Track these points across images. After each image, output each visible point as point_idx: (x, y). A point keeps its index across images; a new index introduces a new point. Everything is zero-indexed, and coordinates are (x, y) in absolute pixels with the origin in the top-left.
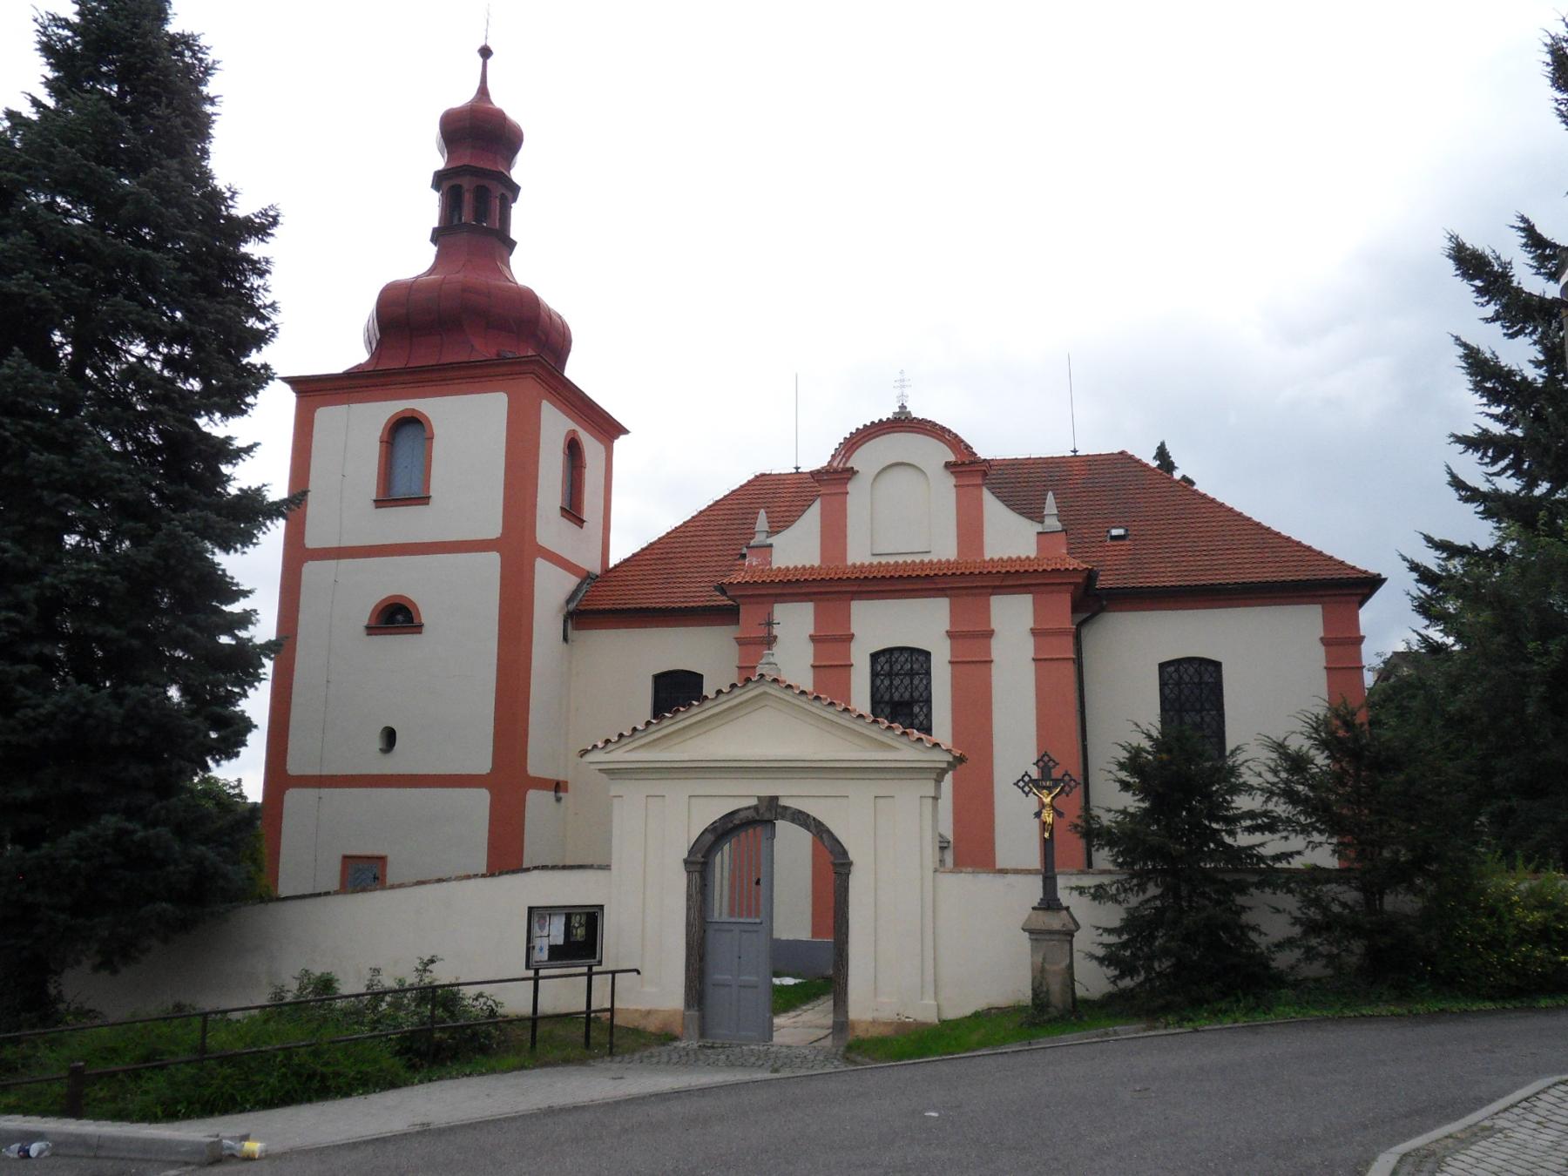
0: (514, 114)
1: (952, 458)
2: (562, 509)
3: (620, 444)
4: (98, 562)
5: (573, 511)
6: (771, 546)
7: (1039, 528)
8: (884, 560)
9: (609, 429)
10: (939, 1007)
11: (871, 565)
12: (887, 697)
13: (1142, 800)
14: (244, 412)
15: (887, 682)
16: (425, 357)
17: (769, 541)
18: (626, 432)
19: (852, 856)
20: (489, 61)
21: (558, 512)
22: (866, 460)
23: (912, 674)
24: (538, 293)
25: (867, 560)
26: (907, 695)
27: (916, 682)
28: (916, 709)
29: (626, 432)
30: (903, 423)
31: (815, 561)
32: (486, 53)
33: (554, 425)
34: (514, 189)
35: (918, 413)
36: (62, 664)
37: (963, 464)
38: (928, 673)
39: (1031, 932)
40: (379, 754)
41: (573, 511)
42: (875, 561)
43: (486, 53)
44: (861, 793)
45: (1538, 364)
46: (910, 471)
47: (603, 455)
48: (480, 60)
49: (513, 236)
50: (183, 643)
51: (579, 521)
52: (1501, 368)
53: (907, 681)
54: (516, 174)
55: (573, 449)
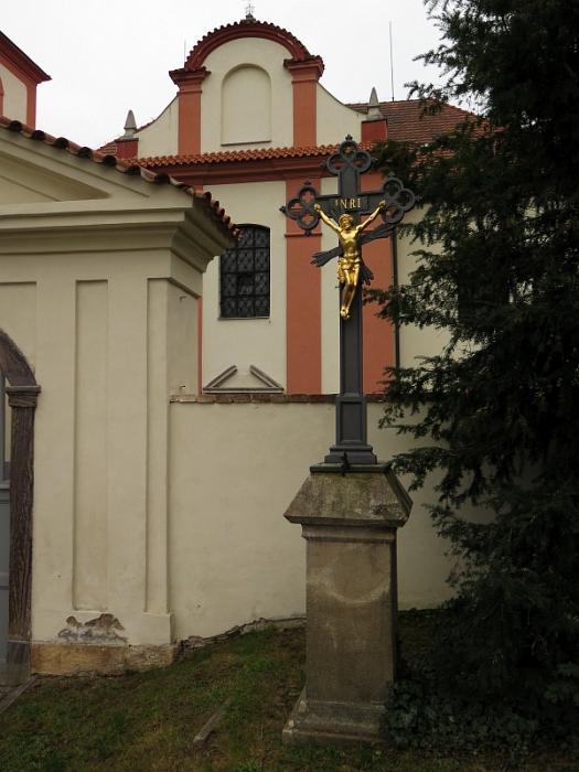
1: (290, 57)
3: (42, 88)
6: (137, 140)
7: (364, 118)
8: (231, 150)
10: (173, 620)
11: (220, 154)
12: (233, 268)
15: (233, 256)
17: (135, 136)
18: (48, 78)
19: (41, 378)
22: (217, 62)
23: (254, 248)
25: (216, 149)
26: (250, 266)
27: (258, 255)
28: (257, 279)
29: (48, 78)
30: (249, 28)
31: (175, 153)
35: (260, 17)
37: (300, 61)
38: (268, 247)
39: (308, 523)
40: (378, 430)
42: (224, 151)
44: (55, 278)
45: (415, 409)
53: (250, 255)
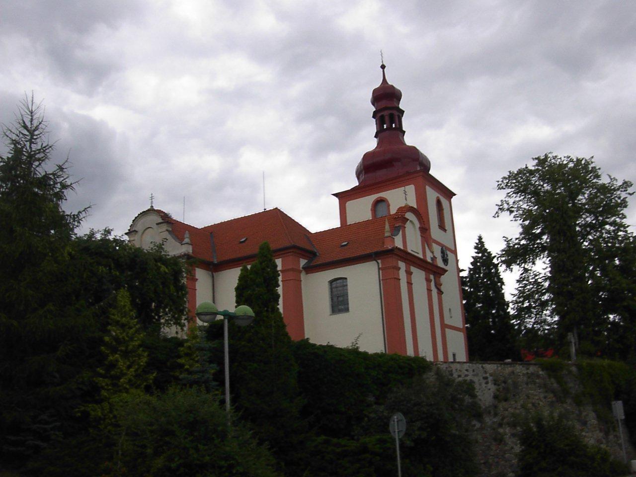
0: (397, 86)
2: (439, 226)
3: (454, 199)
4: (522, 249)
5: (442, 227)
9: (449, 194)
13: (277, 290)
14: (512, 176)
16: (381, 174)
18: (455, 195)
20: (385, 70)
21: (437, 227)
24: (418, 148)
29: (455, 195)
32: (383, 67)
33: (432, 195)
34: (402, 112)
36: (534, 299)
41: (442, 227)
43: (383, 67)
46: (149, 229)
47: (449, 205)
48: (382, 70)
49: (404, 129)
50: (543, 290)
51: (445, 230)
52: (562, 166)
54: (402, 106)
55: (439, 203)
